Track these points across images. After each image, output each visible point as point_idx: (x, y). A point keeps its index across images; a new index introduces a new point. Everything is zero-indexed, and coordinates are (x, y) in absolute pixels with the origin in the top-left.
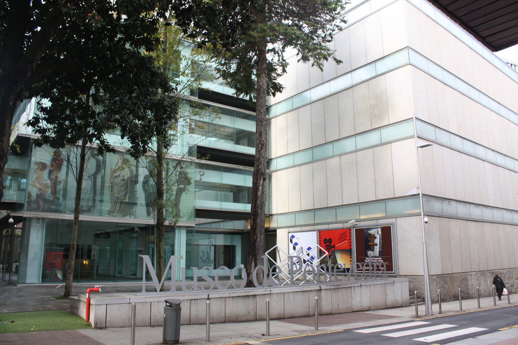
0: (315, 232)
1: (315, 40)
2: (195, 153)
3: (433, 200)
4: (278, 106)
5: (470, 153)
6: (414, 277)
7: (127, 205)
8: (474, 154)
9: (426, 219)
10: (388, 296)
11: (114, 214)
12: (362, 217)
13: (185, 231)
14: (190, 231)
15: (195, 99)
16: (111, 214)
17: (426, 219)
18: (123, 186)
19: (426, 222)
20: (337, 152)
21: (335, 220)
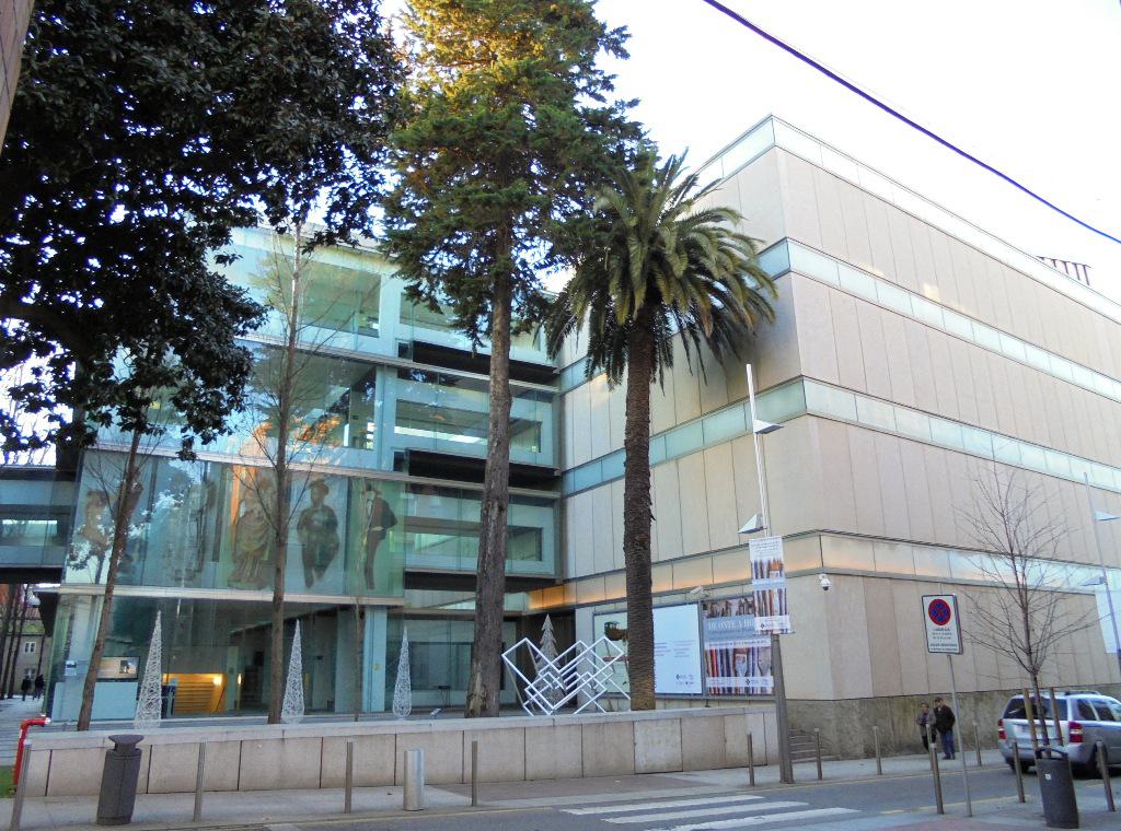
0: (696, 606)
1: (296, 202)
2: (407, 465)
3: (850, 542)
4: (575, 368)
5: (949, 444)
6: (810, 703)
7: (271, 565)
8: (959, 447)
9: (825, 581)
10: (728, 743)
11: (239, 585)
12: (719, 580)
13: (385, 615)
14: (396, 615)
15: (408, 363)
16: (235, 584)
17: (825, 581)
18: (256, 532)
19: (826, 588)
20: (673, 452)
21: (671, 589)
